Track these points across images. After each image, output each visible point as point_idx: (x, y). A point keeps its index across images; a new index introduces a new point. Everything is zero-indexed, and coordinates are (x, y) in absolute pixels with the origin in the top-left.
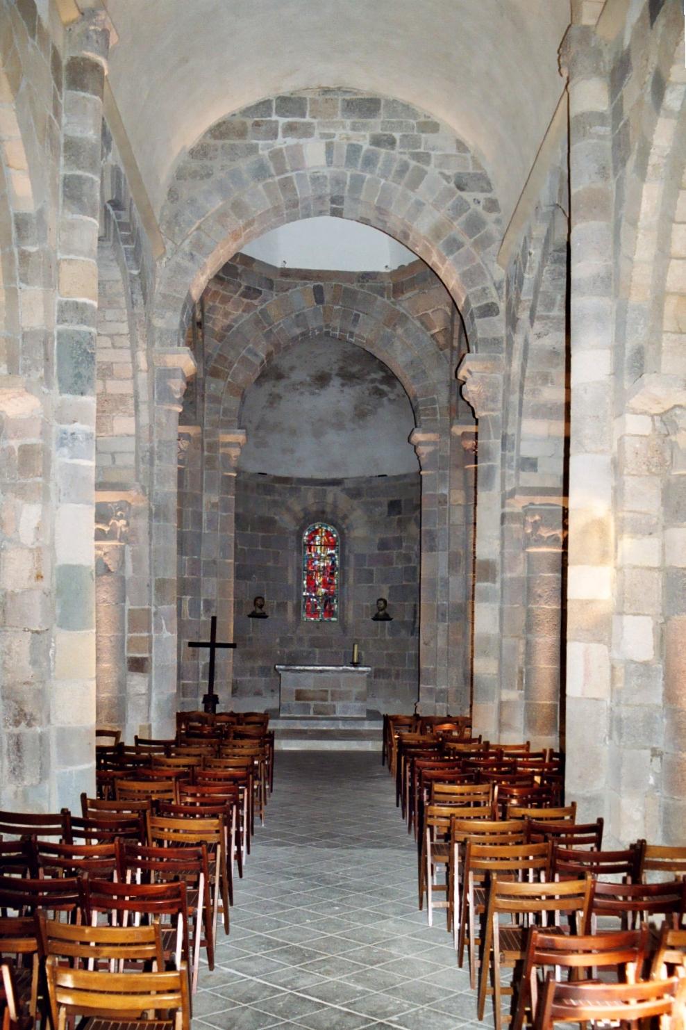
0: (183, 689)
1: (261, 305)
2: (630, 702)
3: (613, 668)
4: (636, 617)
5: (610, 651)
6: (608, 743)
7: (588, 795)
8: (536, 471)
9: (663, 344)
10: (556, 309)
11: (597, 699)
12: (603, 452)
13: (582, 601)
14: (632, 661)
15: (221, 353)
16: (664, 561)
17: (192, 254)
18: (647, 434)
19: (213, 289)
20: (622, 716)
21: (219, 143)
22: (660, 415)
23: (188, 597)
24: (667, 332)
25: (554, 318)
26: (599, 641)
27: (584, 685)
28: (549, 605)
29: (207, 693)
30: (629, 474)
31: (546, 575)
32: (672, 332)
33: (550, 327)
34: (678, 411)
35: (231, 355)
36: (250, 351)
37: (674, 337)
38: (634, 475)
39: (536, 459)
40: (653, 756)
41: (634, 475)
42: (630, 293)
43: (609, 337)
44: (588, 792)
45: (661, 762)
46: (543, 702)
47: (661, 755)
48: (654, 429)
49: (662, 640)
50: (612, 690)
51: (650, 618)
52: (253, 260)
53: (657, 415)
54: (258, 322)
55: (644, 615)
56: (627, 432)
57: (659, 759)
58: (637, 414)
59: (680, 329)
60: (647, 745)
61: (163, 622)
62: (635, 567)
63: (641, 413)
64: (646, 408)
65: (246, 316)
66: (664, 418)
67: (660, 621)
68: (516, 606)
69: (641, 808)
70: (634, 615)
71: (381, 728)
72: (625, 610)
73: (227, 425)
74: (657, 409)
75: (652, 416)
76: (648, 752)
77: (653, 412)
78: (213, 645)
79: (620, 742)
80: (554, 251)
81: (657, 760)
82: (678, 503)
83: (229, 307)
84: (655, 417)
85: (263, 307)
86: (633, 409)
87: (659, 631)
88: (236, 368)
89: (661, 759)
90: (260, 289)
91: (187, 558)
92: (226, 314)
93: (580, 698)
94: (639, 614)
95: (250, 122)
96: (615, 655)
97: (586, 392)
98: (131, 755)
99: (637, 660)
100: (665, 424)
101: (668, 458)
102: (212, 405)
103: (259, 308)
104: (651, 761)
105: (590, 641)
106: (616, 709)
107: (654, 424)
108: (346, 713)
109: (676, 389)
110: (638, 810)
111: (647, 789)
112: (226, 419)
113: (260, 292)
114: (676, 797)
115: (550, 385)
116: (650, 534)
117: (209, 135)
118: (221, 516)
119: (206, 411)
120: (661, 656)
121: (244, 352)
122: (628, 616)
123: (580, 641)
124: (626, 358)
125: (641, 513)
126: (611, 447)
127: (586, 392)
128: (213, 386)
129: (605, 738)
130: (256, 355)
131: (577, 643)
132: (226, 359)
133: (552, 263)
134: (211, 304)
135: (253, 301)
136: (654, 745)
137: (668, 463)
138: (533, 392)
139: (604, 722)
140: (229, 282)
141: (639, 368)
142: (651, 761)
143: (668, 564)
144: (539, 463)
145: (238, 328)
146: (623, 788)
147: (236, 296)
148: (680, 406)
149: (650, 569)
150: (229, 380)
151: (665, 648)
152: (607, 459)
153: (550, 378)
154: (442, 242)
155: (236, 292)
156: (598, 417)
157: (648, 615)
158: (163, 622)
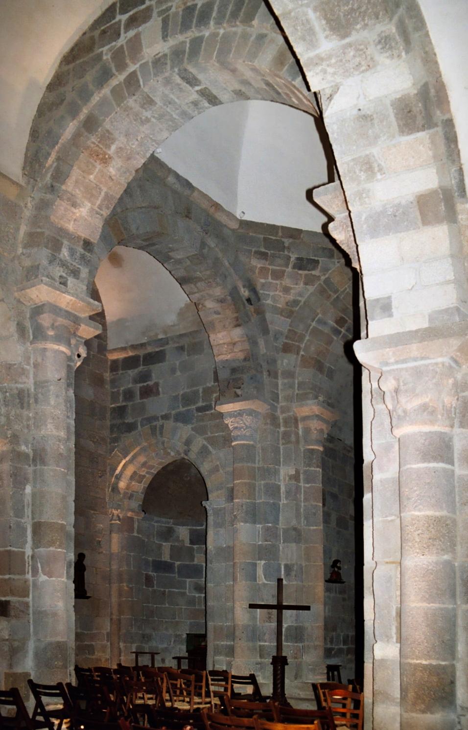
0: (260, 650)
1: (325, 275)
8: (391, 315)
10: (321, 35)
15: (291, 328)
17: (52, 186)
19: (259, 266)
21: (71, 66)
23: (263, 562)
25: (329, 57)
28: (419, 510)
29: (275, 654)
31: (415, 466)
33: (334, 74)
35: (300, 329)
36: (320, 322)
39: (389, 298)
46: (415, 661)
52: (299, 231)
54: (322, 291)
61: (39, 565)
65: (311, 289)
68: (389, 518)
73: (302, 398)
78: (280, 607)
83: (287, 282)
85: (327, 276)
88: (308, 340)
90: (316, 258)
91: (261, 526)
92: (286, 290)
95: (96, 33)
102: (286, 381)
103: (323, 278)
112: (301, 392)
113: (317, 262)
115: (379, 176)
117: (64, 63)
118: (304, 487)
119: (280, 387)
121: (314, 324)
128: (285, 361)
130: (325, 323)
132: (296, 333)
134: (263, 281)
135: (313, 272)
138: (360, 194)
140: (273, 256)
144: (394, 304)
145: (305, 303)
147: (290, 269)
150: (302, 353)
153: (375, 165)
154: (286, 67)
155: (287, 266)
158: (39, 565)
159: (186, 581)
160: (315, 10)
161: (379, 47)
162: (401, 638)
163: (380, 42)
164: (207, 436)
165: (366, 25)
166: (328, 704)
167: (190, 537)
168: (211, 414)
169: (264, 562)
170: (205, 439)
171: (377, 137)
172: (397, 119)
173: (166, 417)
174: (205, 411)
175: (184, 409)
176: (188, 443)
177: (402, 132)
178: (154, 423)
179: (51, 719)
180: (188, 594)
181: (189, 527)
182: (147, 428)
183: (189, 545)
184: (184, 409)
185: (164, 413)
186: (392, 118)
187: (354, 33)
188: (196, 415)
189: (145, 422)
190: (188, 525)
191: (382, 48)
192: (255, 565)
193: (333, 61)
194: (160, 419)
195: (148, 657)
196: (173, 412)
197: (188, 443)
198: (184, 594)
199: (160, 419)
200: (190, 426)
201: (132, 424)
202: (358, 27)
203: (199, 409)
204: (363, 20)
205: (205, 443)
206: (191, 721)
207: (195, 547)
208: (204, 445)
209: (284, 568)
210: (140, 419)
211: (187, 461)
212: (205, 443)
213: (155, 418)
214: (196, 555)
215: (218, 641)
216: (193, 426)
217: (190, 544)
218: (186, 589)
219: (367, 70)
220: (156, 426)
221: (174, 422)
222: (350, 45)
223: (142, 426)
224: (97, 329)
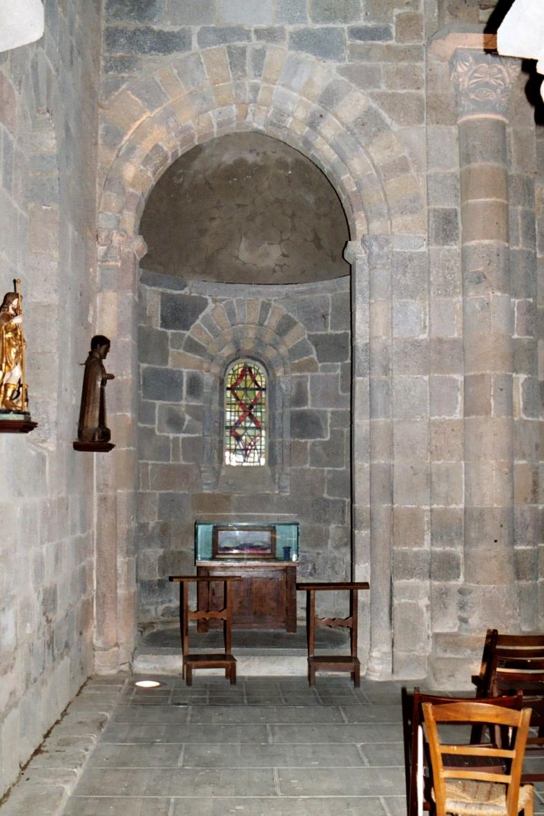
159: (153, 406)
162: (371, 633)
164: (376, 90)
167: (162, 311)
168: (388, 47)
169: (526, 376)
170: (371, 95)
173: (269, 35)
174: (373, 39)
175: (318, 26)
176: (329, 98)
178: (239, 44)
180: (157, 433)
181: (160, 290)
182: (219, 51)
183: (159, 329)
184: (318, 26)
185: (264, 26)
188: (348, 43)
189: (211, 37)
190: (160, 285)
192: (510, 380)
194: (253, 36)
196: (289, 28)
197: (329, 98)
198: (152, 431)
199: (253, 36)
200: (333, 64)
201: (173, 35)
203: (357, 33)
205: (374, 105)
206: (409, 723)
207: (170, 332)
208: (370, 108)
209: (154, 420)
210: (196, 29)
211: (133, 136)
212: (374, 105)
213: (240, 32)
214: (171, 350)
215: (405, 544)
216: (342, 64)
217: (162, 326)
218: (153, 423)
220: (243, 51)
221: (290, 48)
223: (202, 43)
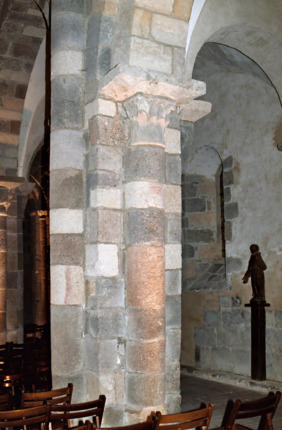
2: (103, 306)
3: (87, 283)
4: (107, 245)
5: (84, 270)
6: (84, 336)
7: (72, 376)
9: (132, 44)
10: (8, 52)
11: (76, 306)
12: (77, 129)
13: (63, 234)
14: (103, 277)
16: (124, 205)
18: (113, 116)
20: (99, 316)
22: (122, 102)
24: (134, 36)
25: (6, 59)
26: (77, 264)
27: (66, 296)
30: (101, 144)
32: (137, 36)
33: (3, 65)
34: (139, 98)
37: (139, 40)
38: (104, 145)
40: (119, 343)
41: (104, 145)
42: (104, 8)
43: (82, 42)
44: (71, 374)
45: (125, 347)
47: (124, 342)
48: (118, 113)
49: (124, 261)
50: (87, 299)
51: (115, 246)
53: (119, 102)
55: (112, 243)
56: (99, 112)
57: (123, 345)
58: (106, 100)
59: (143, 35)
60: (115, 335)
62: (105, 209)
63: (109, 100)
64: (113, 96)
66: (125, 104)
67: (122, 248)
69: (112, 381)
70: (105, 243)
71: (19, 343)
72: (99, 240)
74: (121, 97)
75: (116, 102)
76: (116, 341)
77: (117, 99)
79: (97, 335)
80: (12, 9)
81: (122, 346)
82: (137, 165)
84: (118, 104)
86: (103, 95)
87: (122, 254)
89: (125, 345)
93: (63, 305)
94: (108, 243)
96: (90, 273)
97: (65, 83)
98: (48, 123)
99: (107, 276)
100: (125, 110)
101: (127, 135)
104: (118, 347)
105: (70, 264)
106: (92, 312)
107: (117, 109)
108: (249, 312)
109: (141, 78)
110: (110, 383)
111: (116, 367)
114: (139, 372)
116: (115, 186)
120: (124, 273)
122: (102, 245)
123: (62, 264)
124: (99, 56)
125: (109, 171)
126: (83, 125)
127: (65, 83)
129: (82, 333)
131: (60, 266)
133: (9, 18)
136: (120, 336)
137: (127, 138)
139: (81, 321)
141: (108, 65)
142: (118, 347)
143: (128, 206)
146: (100, 369)
148: (141, 94)
149: (115, 210)
151: (126, 266)
152: (81, 134)
156: (74, 102)
157: (114, 244)
160: (13, 44)
161: (26, 66)
163: (26, 65)
165: (26, 58)
166: (167, 394)
171: (5, 93)
172: (16, 91)
177: (16, 96)
179: (251, 277)
186: (15, 89)
187: (20, 57)
191: (26, 67)
193: (6, 61)
195: (166, 273)
202: (23, 56)
204: (27, 56)
219: (15, 70)
222: (15, 60)
224: (174, 109)
